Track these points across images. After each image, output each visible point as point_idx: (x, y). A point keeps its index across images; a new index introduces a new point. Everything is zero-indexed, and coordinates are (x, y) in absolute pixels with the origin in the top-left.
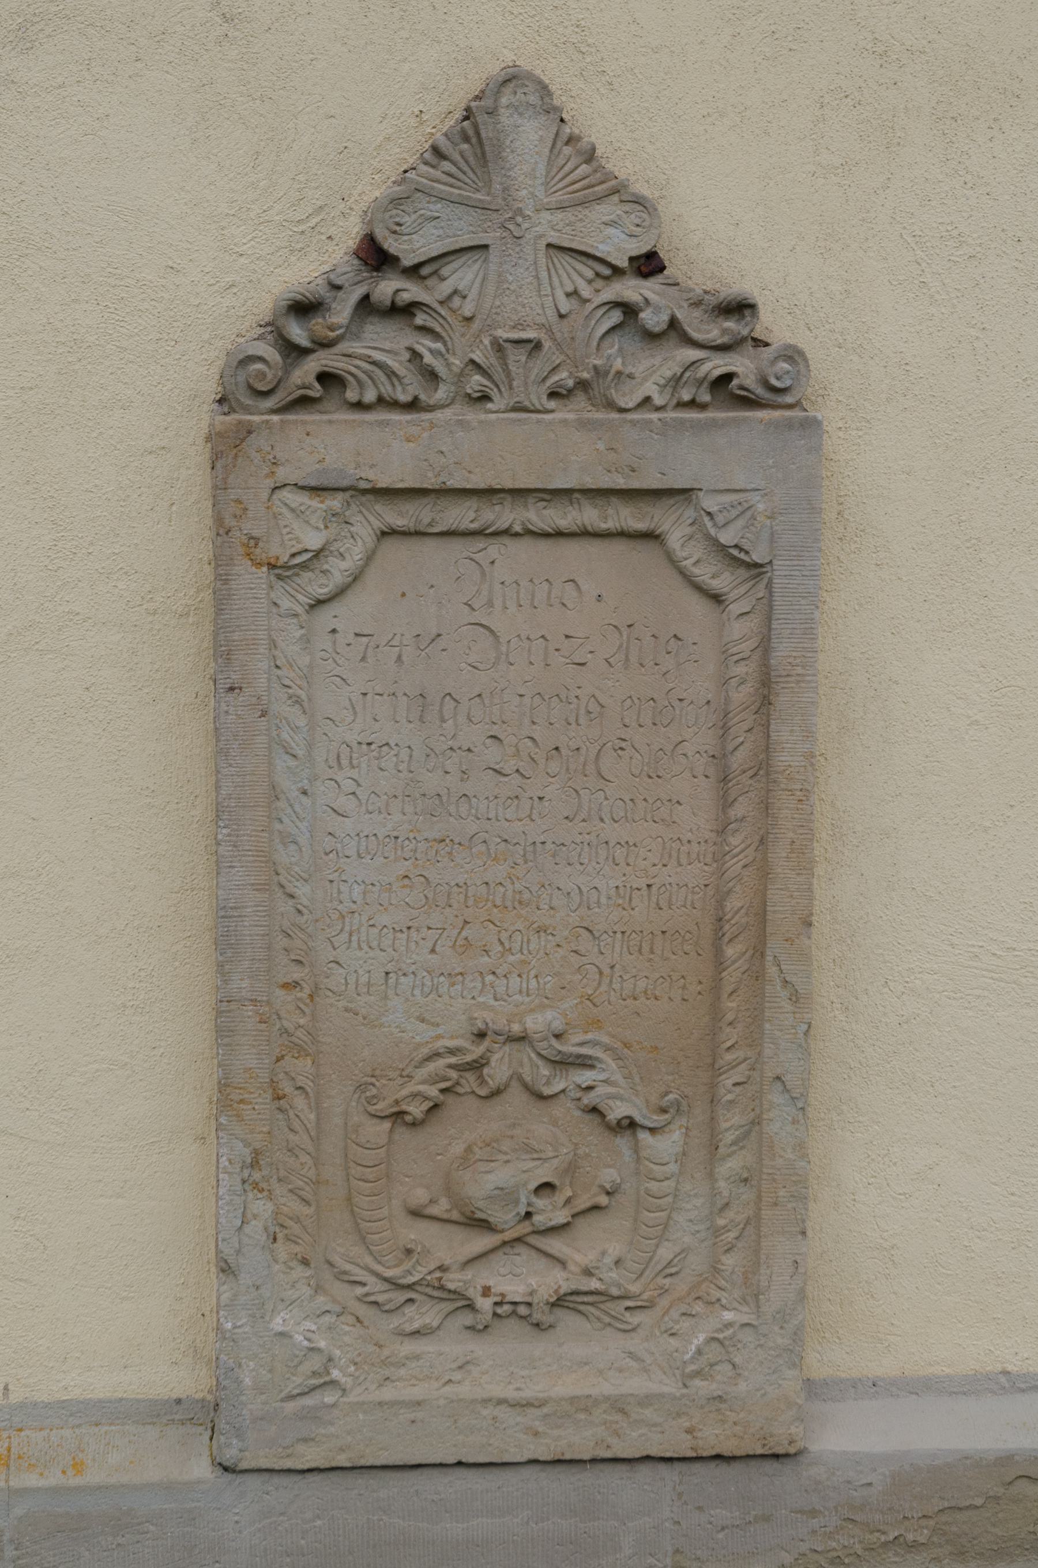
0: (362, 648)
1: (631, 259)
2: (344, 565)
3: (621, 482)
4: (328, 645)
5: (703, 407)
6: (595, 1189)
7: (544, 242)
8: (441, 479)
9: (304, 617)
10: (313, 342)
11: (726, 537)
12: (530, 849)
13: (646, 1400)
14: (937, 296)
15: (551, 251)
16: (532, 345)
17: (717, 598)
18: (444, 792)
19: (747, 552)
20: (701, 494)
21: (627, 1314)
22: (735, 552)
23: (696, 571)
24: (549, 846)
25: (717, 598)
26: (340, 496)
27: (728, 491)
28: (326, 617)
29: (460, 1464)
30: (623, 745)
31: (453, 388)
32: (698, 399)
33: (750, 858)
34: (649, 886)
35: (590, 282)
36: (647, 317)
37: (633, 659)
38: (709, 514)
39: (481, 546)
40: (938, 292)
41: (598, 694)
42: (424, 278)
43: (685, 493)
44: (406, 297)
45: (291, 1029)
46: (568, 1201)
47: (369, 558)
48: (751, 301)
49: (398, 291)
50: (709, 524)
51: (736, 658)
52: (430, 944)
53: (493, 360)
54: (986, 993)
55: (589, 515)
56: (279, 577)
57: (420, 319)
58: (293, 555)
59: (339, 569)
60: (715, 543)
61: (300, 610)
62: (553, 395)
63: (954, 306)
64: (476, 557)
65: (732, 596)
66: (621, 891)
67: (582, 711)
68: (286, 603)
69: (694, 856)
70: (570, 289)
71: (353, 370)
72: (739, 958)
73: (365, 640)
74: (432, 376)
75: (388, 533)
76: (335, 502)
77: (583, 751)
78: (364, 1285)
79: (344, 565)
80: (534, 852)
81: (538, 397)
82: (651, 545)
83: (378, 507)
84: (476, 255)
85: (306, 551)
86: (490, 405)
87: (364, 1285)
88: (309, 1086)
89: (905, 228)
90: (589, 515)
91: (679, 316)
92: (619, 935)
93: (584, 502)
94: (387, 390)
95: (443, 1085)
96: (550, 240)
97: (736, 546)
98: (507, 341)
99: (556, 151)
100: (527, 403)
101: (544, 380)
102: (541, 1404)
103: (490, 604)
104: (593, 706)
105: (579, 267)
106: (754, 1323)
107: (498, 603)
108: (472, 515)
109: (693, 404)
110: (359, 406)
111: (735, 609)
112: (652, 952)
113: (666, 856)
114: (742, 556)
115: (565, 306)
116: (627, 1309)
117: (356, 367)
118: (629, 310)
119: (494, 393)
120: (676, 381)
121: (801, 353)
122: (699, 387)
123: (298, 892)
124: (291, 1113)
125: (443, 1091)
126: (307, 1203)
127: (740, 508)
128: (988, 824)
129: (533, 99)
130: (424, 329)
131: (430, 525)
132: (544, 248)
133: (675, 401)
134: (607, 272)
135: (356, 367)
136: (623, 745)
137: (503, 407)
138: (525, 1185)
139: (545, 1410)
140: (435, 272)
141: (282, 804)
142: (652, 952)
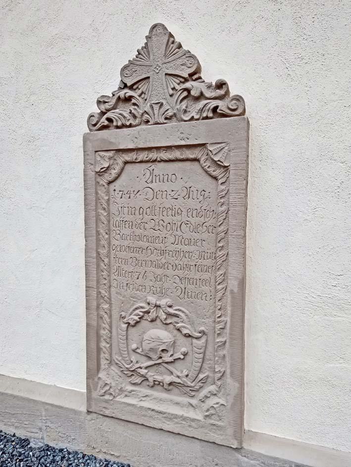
0: (121, 195)
1: (189, 74)
2: (115, 171)
3: (183, 143)
4: (113, 194)
5: (211, 118)
6: (179, 353)
7: (164, 73)
8: (136, 145)
9: (106, 186)
10: (106, 110)
11: (216, 159)
12: (162, 252)
13: (193, 420)
14: (294, 78)
15: (167, 76)
16: (159, 105)
17: (215, 178)
18: (140, 235)
19: (222, 163)
20: (208, 145)
21: (191, 392)
22: (219, 163)
23: (208, 170)
24: (167, 251)
25: (215, 178)
26: (112, 152)
27: (216, 143)
28: (112, 186)
29: (142, 425)
30: (188, 223)
31: (140, 119)
32: (208, 116)
33: (225, 259)
34: (196, 265)
35: (179, 84)
36: (193, 93)
37: (191, 196)
38: (210, 151)
39: (150, 165)
40: (294, 77)
41: (181, 207)
42: (135, 90)
43: (204, 145)
44: (127, 95)
45: (103, 296)
46: (172, 355)
47: (122, 169)
48: (224, 82)
49: (126, 93)
50: (211, 154)
51: (220, 196)
52: (137, 276)
53: (150, 110)
54: (310, 309)
55: (177, 154)
56: (99, 175)
57: (133, 101)
58: (102, 168)
59: (114, 173)
60: (213, 160)
61: (105, 184)
62: (166, 119)
63: (300, 81)
64: (149, 168)
65: (219, 177)
66: (187, 266)
67: (176, 213)
68: (101, 182)
69: (209, 257)
70: (172, 86)
71: (115, 117)
72: (221, 290)
73: (122, 192)
74: (135, 117)
75: (126, 163)
76: (111, 154)
77: (176, 224)
78: (122, 368)
79: (115, 171)
80: (163, 253)
81: (162, 120)
82: (196, 163)
83: (123, 155)
84: (147, 80)
85: (105, 168)
86: (149, 123)
87: (122, 368)
88: (108, 312)
89: (282, 57)
90: (177, 154)
91: (203, 90)
92: (187, 279)
93: (176, 151)
94: (124, 122)
95: (139, 317)
96: (166, 72)
97: (219, 161)
98: (153, 104)
99: (168, 46)
100: (159, 122)
101: (164, 114)
102: (165, 413)
103: (152, 182)
104: (179, 211)
105: (175, 79)
106: (226, 405)
107: (154, 181)
108: (146, 156)
109: (207, 118)
110: (117, 127)
111: (220, 181)
112: (196, 284)
113: (200, 256)
114: (221, 164)
115: (171, 92)
116: (190, 390)
117: (115, 115)
118: (188, 90)
119: (150, 119)
120: (201, 110)
121: (241, 97)
122: (208, 112)
123: (105, 260)
124: (104, 318)
125: (139, 318)
126: (108, 343)
127: (220, 149)
128: (311, 254)
129: (162, 31)
130: (134, 104)
131: (136, 159)
132: (164, 75)
133: (201, 117)
134: (183, 80)
135: (115, 115)
136: (188, 223)
137: (152, 123)
138: (159, 349)
139: (165, 415)
140: (137, 87)
141: (101, 236)
142: (196, 284)
